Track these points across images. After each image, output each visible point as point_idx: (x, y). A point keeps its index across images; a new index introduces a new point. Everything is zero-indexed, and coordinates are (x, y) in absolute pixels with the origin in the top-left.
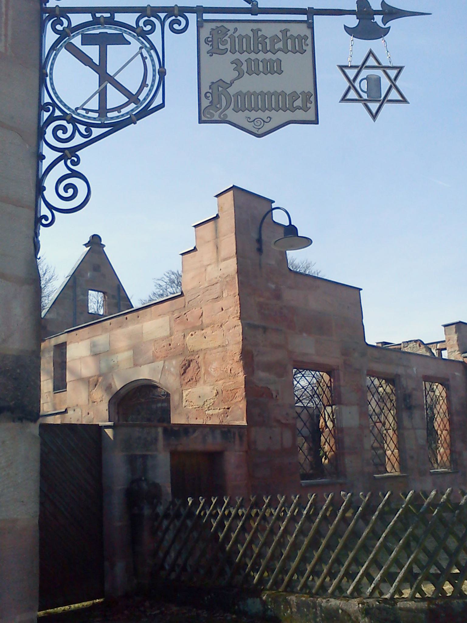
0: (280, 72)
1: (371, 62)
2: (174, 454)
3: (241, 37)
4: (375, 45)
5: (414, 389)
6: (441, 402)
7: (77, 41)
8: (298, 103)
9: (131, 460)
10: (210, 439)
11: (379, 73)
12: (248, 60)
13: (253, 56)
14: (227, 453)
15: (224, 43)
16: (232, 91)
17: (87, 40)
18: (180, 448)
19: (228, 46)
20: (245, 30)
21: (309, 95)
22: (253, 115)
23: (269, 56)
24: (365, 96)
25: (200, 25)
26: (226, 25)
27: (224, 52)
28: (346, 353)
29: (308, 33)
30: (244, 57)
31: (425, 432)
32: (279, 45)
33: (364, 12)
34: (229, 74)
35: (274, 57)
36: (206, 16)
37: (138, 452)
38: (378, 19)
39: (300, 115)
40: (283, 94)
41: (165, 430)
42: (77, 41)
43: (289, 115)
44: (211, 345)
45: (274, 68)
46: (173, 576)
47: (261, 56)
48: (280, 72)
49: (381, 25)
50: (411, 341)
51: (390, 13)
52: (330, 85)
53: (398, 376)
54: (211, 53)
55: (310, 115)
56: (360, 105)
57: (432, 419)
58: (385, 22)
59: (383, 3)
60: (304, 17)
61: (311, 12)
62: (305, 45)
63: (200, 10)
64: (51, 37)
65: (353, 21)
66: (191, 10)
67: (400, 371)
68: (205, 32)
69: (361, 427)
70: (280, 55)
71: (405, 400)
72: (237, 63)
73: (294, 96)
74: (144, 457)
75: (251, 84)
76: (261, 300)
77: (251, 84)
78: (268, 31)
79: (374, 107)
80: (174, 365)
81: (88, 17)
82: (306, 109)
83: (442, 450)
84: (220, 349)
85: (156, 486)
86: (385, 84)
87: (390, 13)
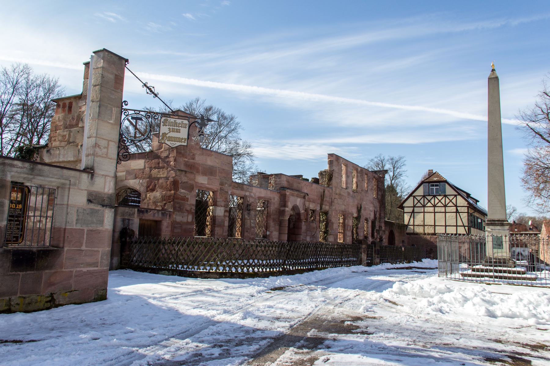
0: (180, 132)
2: (141, 220)
7: (130, 118)
8: (183, 141)
9: (123, 220)
10: (156, 215)
16: (167, 136)
17: (133, 118)
18: (144, 218)
22: (172, 142)
23: (177, 128)
27: (166, 125)
34: (167, 131)
37: (126, 218)
41: (138, 210)
42: (130, 118)
44: (162, 176)
45: (178, 131)
46: (136, 264)
47: (176, 128)
48: (180, 132)
53: (246, 196)
54: (163, 125)
64: (123, 116)
67: (247, 194)
70: (180, 128)
72: (169, 129)
73: (182, 139)
74: (129, 220)
75: (172, 134)
76: (186, 160)
77: (172, 134)
80: (144, 182)
81: (133, 112)
85: (133, 231)
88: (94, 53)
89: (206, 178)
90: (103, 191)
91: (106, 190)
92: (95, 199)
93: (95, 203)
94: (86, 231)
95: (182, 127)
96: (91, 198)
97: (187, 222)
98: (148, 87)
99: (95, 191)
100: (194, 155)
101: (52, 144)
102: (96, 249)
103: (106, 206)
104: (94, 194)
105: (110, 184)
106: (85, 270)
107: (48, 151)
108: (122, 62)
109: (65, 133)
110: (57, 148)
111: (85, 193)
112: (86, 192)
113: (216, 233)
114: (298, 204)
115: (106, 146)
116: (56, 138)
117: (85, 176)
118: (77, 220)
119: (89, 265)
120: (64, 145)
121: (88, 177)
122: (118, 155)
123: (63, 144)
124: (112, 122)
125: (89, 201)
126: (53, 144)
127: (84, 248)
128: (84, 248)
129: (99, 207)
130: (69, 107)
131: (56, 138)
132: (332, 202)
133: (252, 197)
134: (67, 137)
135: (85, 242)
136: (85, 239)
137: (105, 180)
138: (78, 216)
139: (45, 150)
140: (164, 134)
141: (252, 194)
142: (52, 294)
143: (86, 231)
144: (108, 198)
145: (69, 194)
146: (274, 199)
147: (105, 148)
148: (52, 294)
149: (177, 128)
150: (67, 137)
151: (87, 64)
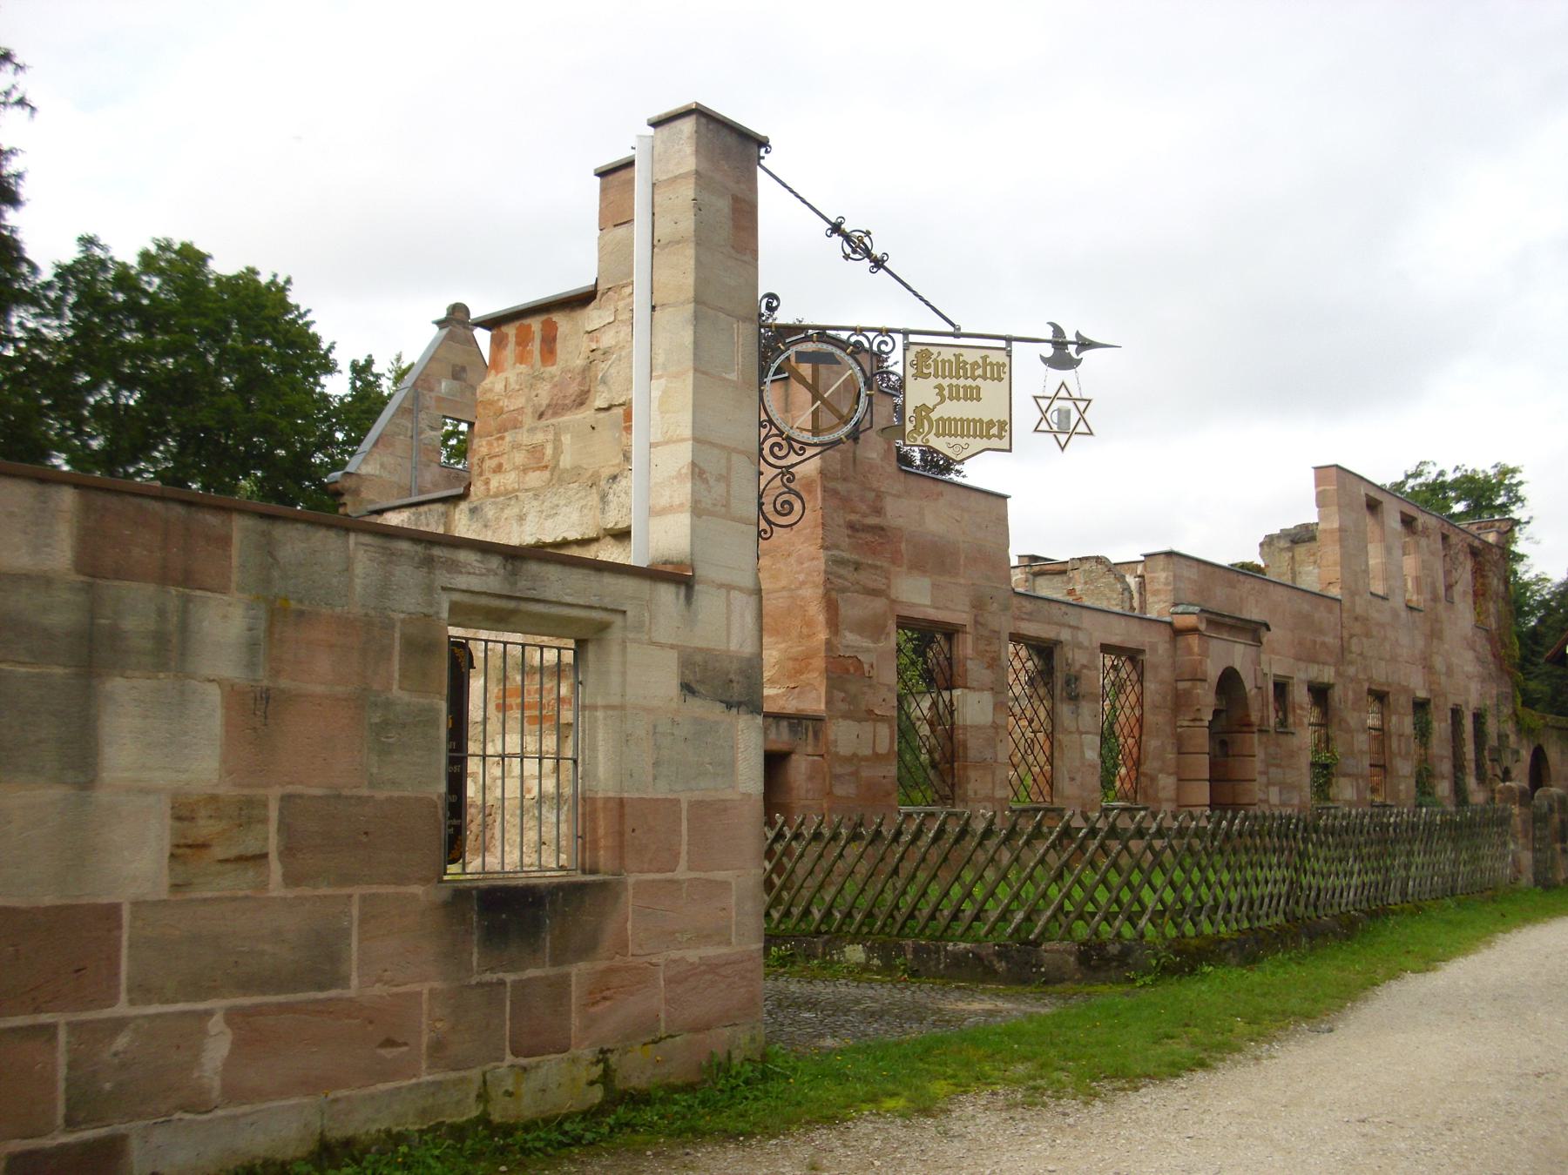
0: (979, 399)
1: (1063, 393)
3: (943, 362)
4: (1066, 375)
5: (1084, 666)
6: (1129, 689)
8: (994, 431)
11: (1070, 404)
12: (950, 386)
13: (954, 381)
14: (794, 757)
15: (928, 367)
16: (934, 416)
19: (932, 370)
20: (948, 354)
21: (1002, 425)
22: (953, 441)
23: (970, 382)
24: (1055, 428)
25: (906, 348)
26: (931, 349)
27: (927, 376)
28: (978, 605)
29: (1006, 360)
30: (946, 382)
31: (1098, 739)
32: (979, 372)
33: (1059, 343)
34: (931, 399)
35: (974, 384)
36: (912, 338)
38: (1072, 349)
39: (995, 443)
40: (981, 421)
43: (985, 443)
45: (973, 395)
47: (962, 382)
48: (979, 399)
49: (1074, 355)
50: (1087, 558)
51: (1085, 344)
52: (1025, 416)
53: (1058, 643)
54: (915, 376)
55: (1004, 444)
56: (1051, 436)
57: (301, 783)
58: (1078, 352)
59: (1078, 334)
60: (1002, 344)
61: (1009, 340)
62: (1000, 372)
63: (906, 333)
65: (1048, 351)
66: (897, 331)
67: (1065, 635)
68: (911, 356)
69: (995, 726)
70: (979, 382)
71: (1068, 683)
72: (940, 387)
73: (991, 424)
78: (970, 357)
79: (1063, 438)
82: (1000, 437)
83: (1123, 771)
84: (785, 593)
86: (1074, 416)
87: (1085, 344)
88: (656, 124)
89: (925, 582)
90: (723, 647)
91: (733, 647)
92: (701, 682)
93: (705, 697)
94: (684, 806)
95: (985, 378)
96: (690, 678)
97: (876, 755)
98: (847, 237)
99: (701, 650)
100: (879, 496)
101: (487, 483)
102: (720, 875)
103: (739, 705)
104: (699, 658)
105: (742, 616)
106: (693, 955)
107: (473, 511)
108: (747, 145)
109: (539, 437)
110: (510, 495)
111: (671, 660)
112: (674, 654)
113: (971, 793)
114: (1238, 667)
115: (724, 472)
116: (503, 460)
117: (667, 595)
118: (656, 764)
119: (704, 937)
120: (537, 484)
121: (678, 594)
122: (760, 505)
123: (535, 479)
124: (733, 376)
125: (687, 688)
126: (494, 484)
127: (682, 873)
128: (682, 873)
129: (716, 712)
130: (543, 340)
131: (503, 460)
132: (1342, 648)
133: (1079, 646)
134: (549, 451)
135: (684, 848)
136: (685, 838)
137: (729, 605)
138: (657, 747)
139: (464, 506)
140: (924, 411)
141: (1081, 637)
142: (602, 1052)
143: (684, 806)
144: (741, 672)
145: (624, 663)
146: (1154, 648)
147: (720, 478)
148: (602, 1052)
149: (970, 382)
150: (549, 451)
151: (614, 174)
